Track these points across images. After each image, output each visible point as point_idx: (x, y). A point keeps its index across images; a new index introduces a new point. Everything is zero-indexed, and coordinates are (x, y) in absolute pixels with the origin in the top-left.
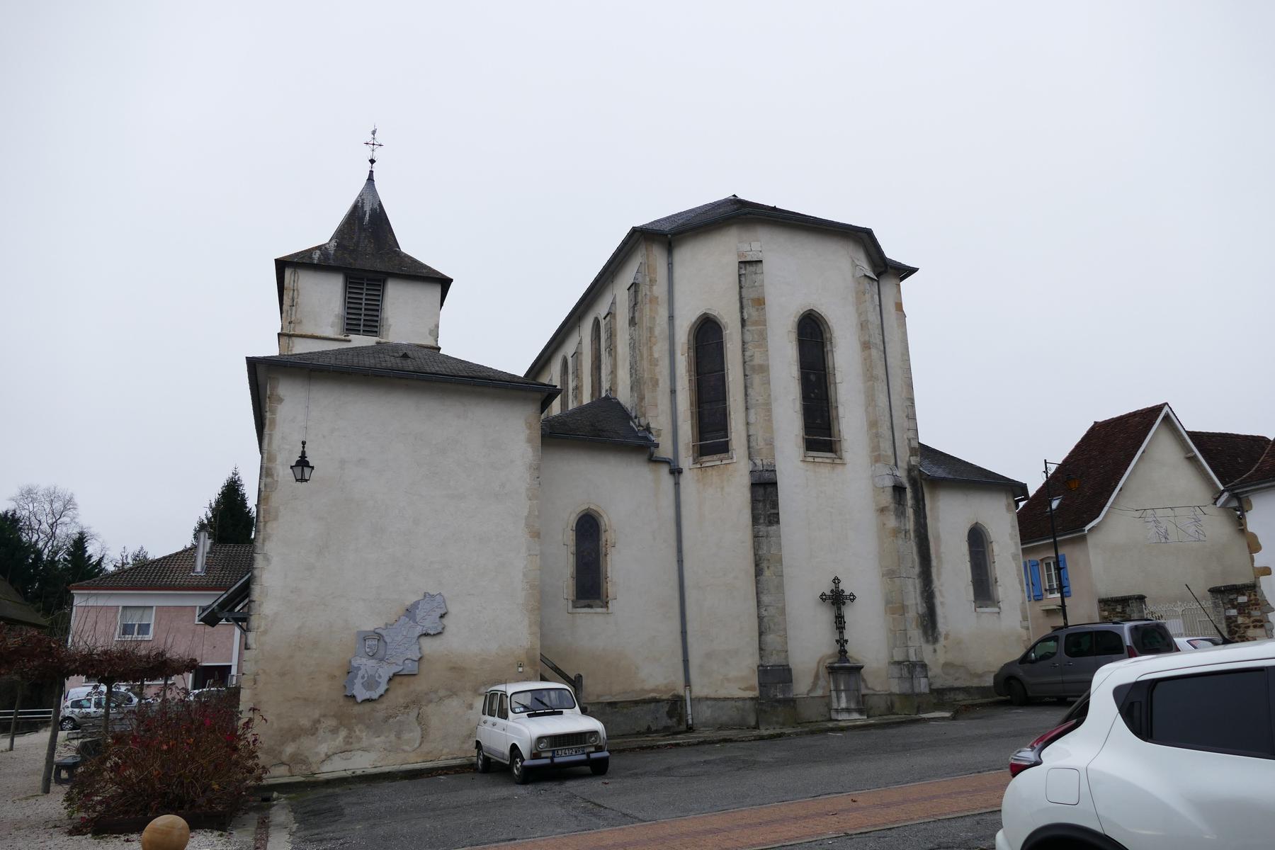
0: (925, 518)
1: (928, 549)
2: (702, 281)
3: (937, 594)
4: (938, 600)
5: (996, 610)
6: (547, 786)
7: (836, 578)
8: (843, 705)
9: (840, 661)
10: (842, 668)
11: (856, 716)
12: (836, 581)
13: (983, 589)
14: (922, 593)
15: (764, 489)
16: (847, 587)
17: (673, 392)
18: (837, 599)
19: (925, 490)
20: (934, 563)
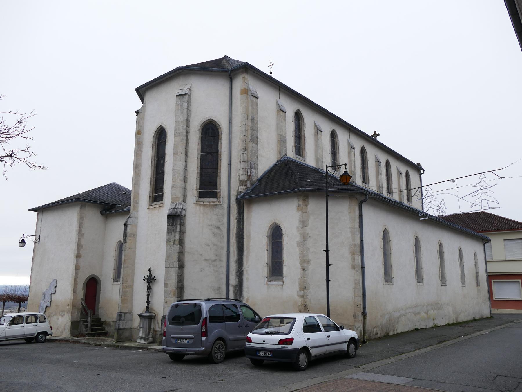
0: (243, 224)
1: (243, 245)
2: (210, 100)
3: (245, 273)
4: (245, 276)
5: (281, 283)
6: (298, 372)
7: (150, 269)
8: (140, 335)
9: (146, 312)
10: (149, 316)
11: (142, 341)
12: (150, 270)
13: (276, 269)
14: (237, 272)
15: (175, 219)
16: (154, 274)
17: (230, 164)
18: (150, 279)
19: (245, 206)
20: (245, 253)
